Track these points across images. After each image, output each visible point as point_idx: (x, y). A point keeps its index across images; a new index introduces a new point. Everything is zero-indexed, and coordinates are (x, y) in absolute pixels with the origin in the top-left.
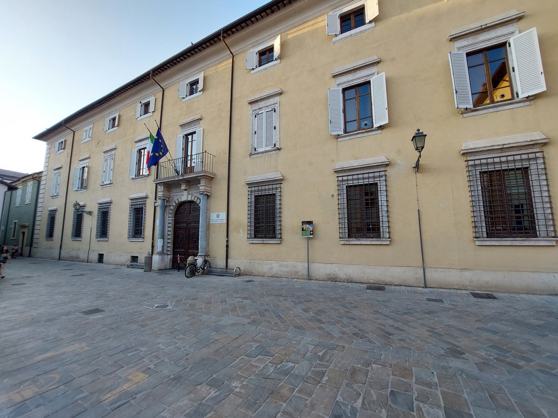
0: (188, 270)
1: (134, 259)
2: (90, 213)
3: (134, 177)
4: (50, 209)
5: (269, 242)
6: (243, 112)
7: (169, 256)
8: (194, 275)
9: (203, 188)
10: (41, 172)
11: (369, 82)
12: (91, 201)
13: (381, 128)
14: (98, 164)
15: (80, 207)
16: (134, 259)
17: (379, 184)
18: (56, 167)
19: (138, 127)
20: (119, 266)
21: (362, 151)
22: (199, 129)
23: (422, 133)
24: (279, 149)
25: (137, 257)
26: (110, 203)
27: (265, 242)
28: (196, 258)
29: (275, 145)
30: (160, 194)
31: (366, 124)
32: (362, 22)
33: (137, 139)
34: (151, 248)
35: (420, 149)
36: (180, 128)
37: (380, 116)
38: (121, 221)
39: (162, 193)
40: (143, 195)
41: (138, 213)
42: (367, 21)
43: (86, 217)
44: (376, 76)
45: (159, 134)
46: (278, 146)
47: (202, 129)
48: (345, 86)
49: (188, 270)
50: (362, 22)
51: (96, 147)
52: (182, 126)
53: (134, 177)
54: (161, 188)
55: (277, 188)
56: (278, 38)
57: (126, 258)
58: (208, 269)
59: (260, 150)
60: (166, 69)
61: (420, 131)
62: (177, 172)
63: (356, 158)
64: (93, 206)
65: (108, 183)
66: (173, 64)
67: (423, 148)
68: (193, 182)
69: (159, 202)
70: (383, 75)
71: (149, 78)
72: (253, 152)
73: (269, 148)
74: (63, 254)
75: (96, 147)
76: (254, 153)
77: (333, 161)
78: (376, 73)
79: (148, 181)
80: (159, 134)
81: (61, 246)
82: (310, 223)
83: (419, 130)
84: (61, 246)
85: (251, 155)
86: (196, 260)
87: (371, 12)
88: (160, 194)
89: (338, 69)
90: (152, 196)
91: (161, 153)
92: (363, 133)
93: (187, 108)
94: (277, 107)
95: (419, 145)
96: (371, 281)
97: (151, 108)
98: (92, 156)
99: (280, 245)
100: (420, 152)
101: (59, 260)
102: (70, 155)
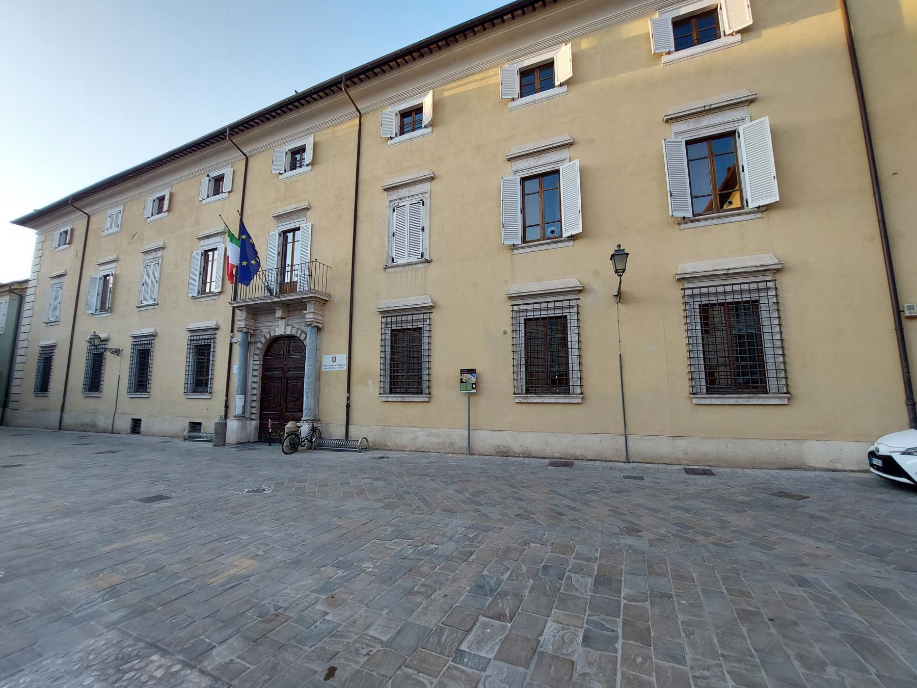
1: (195, 426)
3: (195, 294)
4: (43, 343)
5: (412, 400)
6: (375, 203)
7: (254, 422)
9: (311, 316)
11: (558, 171)
13: (572, 238)
14: (133, 273)
16: (195, 426)
20: (168, 439)
21: (546, 271)
24: (427, 261)
25: (200, 424)
26: (154, 335)
27: (407, 400)
30: (240, 324)
32: (549, 83)
33: (201, 234)
34: (223, 409)
35: (620, 272)
36: (274, 221)
38: (171, 366)
42: (557, 83)
45: (243, 229)
46: (427, 257)
48: (524, 175)
49: (286, 443)
50: (549, 83)
53: (195, 294)
54: (241, 315)
55: (424, 320)
57: (182, 426)
59: (400, 261)
60: (253, 126)
62: (270, 291)
63: (539, 280)
65: (151, 303)
67: (624, 270)
68: (294, 307)
69: (238, 337)
72: (390, 264)
73: (414, 259)
80: (243, 229)
81: (63, 403)
82: (472, 371)
83: (619, 246)
85: (386, 268)
88: (240, 324)
90: (226, 326)
96: (556, 455)
97: (226, 185)
98: (121, 258)
101: (60, 429)
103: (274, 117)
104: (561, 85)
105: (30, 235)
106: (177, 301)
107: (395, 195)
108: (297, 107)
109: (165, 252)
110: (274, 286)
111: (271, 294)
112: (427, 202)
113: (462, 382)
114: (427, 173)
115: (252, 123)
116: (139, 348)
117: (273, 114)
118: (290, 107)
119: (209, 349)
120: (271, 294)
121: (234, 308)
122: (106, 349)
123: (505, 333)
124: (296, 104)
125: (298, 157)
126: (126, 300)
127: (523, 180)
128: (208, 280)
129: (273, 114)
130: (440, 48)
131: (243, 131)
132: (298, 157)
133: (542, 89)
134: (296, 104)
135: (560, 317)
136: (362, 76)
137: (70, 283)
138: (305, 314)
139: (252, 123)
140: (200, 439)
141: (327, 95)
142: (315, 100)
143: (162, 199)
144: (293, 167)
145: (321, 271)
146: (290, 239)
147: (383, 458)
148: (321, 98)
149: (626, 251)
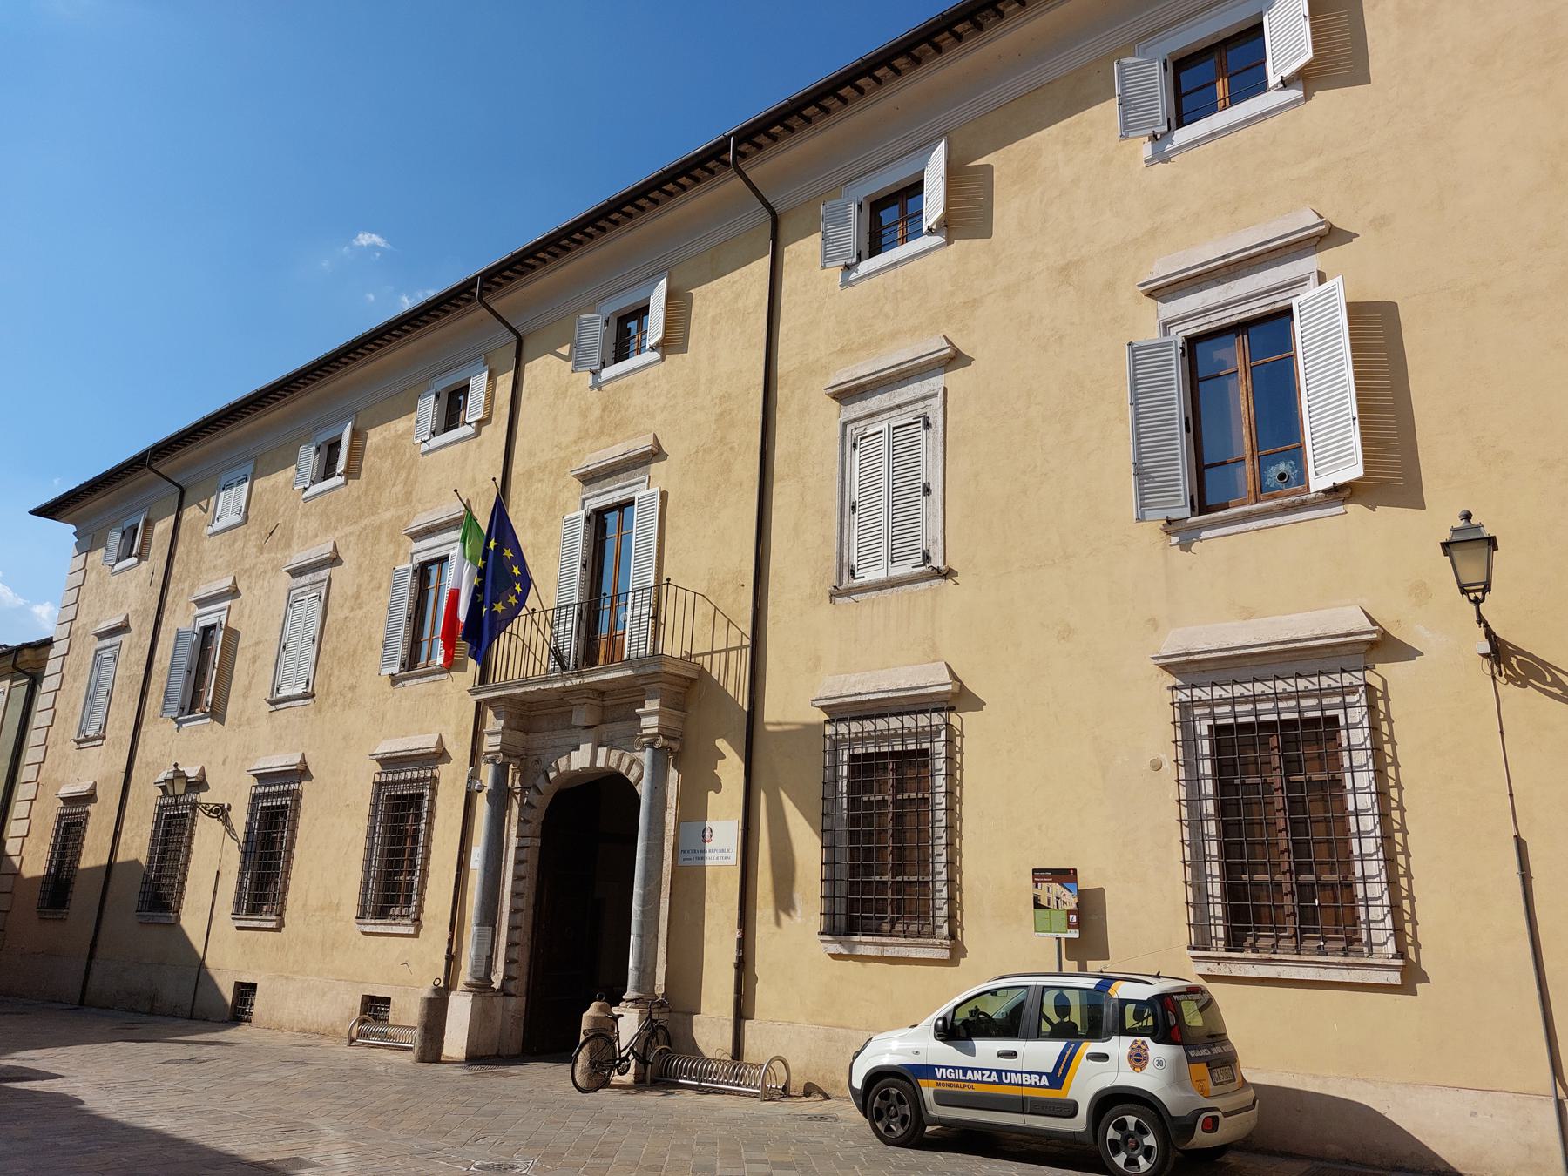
0: (583, 1058)
1: (375, 1007)
2: (221, 813)
3: (395, 670)
4: (68, 790)
5: (903, 952)
6: (810, 425)
7: (512, 1002)
8: (606, 1083)
9: (654, 720)
10: (48, 643)
11: (1287, 312)
12: (229, 758)
13: (1340, 493)
14: (264, 618)
15: (189, 785)
16: (375, 1007)
17: (1342, 722)
18: (104, 626)
19: (423, 472)
20: (315, 1039)
21: (1278, 584)
22: (642, 491)
23: (1478, 527)
24: (946, 574)
25: (387, 1001)
26: (302, 773)
27: (890, 952)
28: (615, 1011)
29: (927, 558)
30: (491, 743)
31: (1282, 476)
32: (1250, 80)
33: (418, 522)
34: (442, 963)
35: (1477, 591)
36: (577, 484)
37: (1333, 447)
38: (332, 849)
39: (497, 739)
40: (424, 742)
41: (400, 815)
42: (1273, 80)
43: (206, 832)
44: (1312, 290)
45: (500, 514)
46: (937, 562)
47: (656, 490)
48: (1193, 328)
49: (583, 1058)
50: (1250, 80)
51: (261, 550)
52: (589, 479)
53: (395, 670)
54: (493, 723)
55: (933, 734)
56: (939, 155)
57: (343, 1008)
58: (665, 1060)
59: (870, 575)
60: (533, 267)
61: (1474, 521)
62: (559, 658)
63: (1248, 614)
64: (233, 789)
65: (298, 690)
66: (557, 251)
67: (1487, 588)
68: (612, 711)
69: (487, 774)
70: (1338, 292)
71: (468, 301)
72: (847, 583)
73: (904, 569)
74: (95, 982)
75: (261, 550)
76: (845, 586)
77: (1153, 623)
78: (1314, 277)
79: (448, 685)
80: (500, 514)
81: (93, 946)
82: (1065, 876)
83: (1467, 516)
84: (93, 946)
85: (836, 593)
86: (616, 1018)
87: (1288, 41)
88: (491, 743)
89: (1163, 267)
90: (459, 750)
91: (513, 600)
92: (1268, 513)
93: (604, 409)
94: (934, 408)
95: (1473, 575)
96: (1332, 1148)
97: (474, 408)
98: (242, 587)
99: (949, 970)
100: (1477, 602)
101: (82, 1003)
102: (159, 579)
103: (580, 242)
104: (1285, 83)
105: (63, 532)
106: (353, 688)
107: (857, 409)
108: (630, 216)
109: (335, 572)
110: (570, 649)
111: (564, 668)
112: (937, 421)
113: (1037, 905)
114: (933, 345)
115: (531, 261)
116: (262, 804)
117: (577, 236)
118: (615, 216)
119: (419, 807)
120: (564, 668)
121: (478, 704)
122: (195, 806)
123: (1157, 766)
124: (628, 209)
125: (633, 325)
126: (250, 681)
127: (1192, 342)
128: (427, 635)
129: (577, 236)
130: (959, 38)
131: (510, 279)
132: (633, 325)
133: (1235, 98)
134: (628, 209)
135: (1314, 722)
136: (776, 129)
137: (133, 646)
138: (639, 718)
139: (531, 261)
140: (386, 1042)
141: (697, 180)
142: (671, 194)
143: (334, 446)
144: (621, 354)
145: (680, 607)
146: (612, 532)
147: (823, 1118)
148: (684, 188)
149: (1488, 531)
